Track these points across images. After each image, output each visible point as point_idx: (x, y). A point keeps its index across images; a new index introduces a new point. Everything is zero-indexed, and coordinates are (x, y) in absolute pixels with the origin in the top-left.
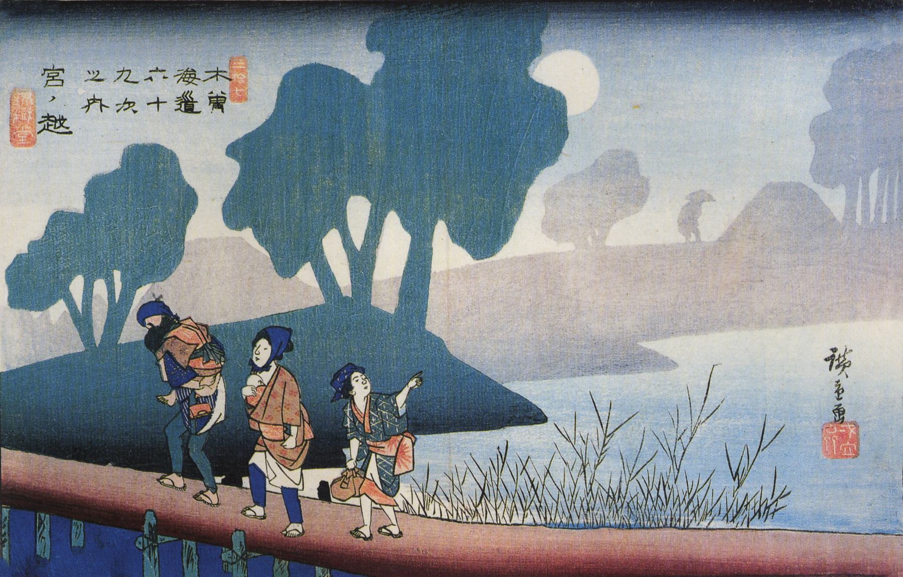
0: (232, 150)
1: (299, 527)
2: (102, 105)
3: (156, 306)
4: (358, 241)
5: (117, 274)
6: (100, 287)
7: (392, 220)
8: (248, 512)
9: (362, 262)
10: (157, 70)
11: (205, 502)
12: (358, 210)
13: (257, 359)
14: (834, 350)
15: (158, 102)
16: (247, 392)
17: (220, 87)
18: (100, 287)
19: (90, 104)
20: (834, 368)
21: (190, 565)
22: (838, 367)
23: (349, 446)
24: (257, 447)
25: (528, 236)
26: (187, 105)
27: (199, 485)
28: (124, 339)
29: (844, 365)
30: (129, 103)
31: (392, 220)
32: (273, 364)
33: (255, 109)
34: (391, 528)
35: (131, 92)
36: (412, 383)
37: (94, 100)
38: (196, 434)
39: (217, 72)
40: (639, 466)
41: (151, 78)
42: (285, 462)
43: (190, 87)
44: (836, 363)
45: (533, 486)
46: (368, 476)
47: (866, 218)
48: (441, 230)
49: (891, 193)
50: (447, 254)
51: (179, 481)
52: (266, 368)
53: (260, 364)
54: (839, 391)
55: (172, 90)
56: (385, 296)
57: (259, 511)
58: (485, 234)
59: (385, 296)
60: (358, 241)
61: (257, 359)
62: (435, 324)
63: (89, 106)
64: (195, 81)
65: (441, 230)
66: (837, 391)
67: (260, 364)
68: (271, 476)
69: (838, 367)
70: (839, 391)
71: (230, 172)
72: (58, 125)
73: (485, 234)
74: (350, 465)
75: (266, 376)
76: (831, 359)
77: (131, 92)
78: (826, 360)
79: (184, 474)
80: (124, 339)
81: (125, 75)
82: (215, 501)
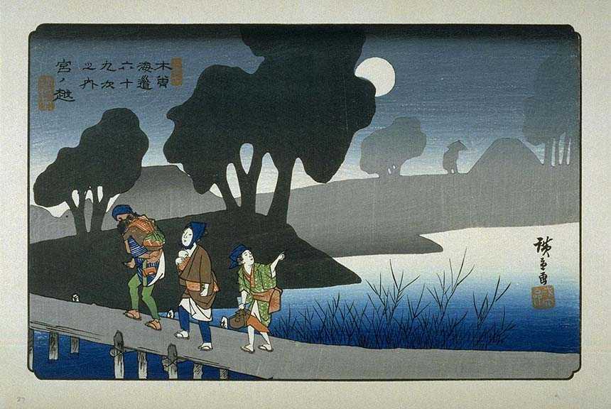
0: (170, 116)
1: (209, 344)
2: (93, 84)
3: (127, 209)
4: (246, 167)
5: (100, 189)
6: (89, 195)
7: (267, 160)
8: (178, 335)
9: (249, 182)
10: (127, 63)
11: (153, 328)
12: (246, 154)
13: (185, 241)
14: (540, 239)
15: (127, 82)
16: (178, 261)
17: (165, 73)
18: (89, 195)
19: (85, 84)
20: (540, 250)
21: (143, 367)
22: (542, 250)
23: (240, 296)
24: (184, 295)
25: (350, 170)
26: (144, 84)
27: (148, 318)
28: (105, 227)
29: (547, 248)
30: (110, 84)
31: (267, 160)
32: (195, 244)
33: (182, 92)
34: (266, 346)
35: (110, 76)
36: (280, 257)
37: (89, 81)
38: (147, 286)
39: (163, 64)
40: (435, 296)
41: (123, 68)
42: (200, 303)
43: (148, 73)
44: (541, 247)
45: (354, 321)
46: (252, 314)
47: (557, 162)
48: (299, 166)
49: (565, 150)
50: (300, 178)
51: (137, 315)
52: (190, 247)
53: (187, 244)
54: (543, 265)
55: (137, 75)
56: (263, 208)
57: (185, 334)
58: (323, 169)
59: (263, 208)
60: (246, 167)
61: (185, 241)
62: (292, 218)
63: (85, 85)
64: (150, 70)
65: (299, 166)
66: (542, 265)
67: (187, 244)
68: (193, 313)
69: (542, 250)
70: (543, 265)
71: (169, 128)
72: (66, 95)
73: (323, 169)
74: (242, 307)
75: (190, 252)
76: (538, 245)
77: (110, 76)
78: (535, 245)
79: (140, 311)
80: (105, 227)
81: (107, 66)
82: (159, 327)
